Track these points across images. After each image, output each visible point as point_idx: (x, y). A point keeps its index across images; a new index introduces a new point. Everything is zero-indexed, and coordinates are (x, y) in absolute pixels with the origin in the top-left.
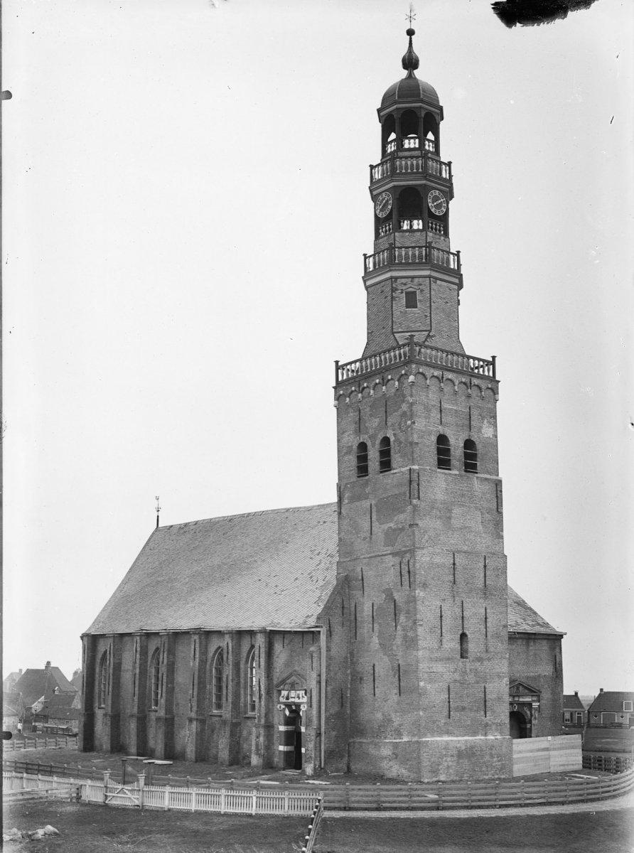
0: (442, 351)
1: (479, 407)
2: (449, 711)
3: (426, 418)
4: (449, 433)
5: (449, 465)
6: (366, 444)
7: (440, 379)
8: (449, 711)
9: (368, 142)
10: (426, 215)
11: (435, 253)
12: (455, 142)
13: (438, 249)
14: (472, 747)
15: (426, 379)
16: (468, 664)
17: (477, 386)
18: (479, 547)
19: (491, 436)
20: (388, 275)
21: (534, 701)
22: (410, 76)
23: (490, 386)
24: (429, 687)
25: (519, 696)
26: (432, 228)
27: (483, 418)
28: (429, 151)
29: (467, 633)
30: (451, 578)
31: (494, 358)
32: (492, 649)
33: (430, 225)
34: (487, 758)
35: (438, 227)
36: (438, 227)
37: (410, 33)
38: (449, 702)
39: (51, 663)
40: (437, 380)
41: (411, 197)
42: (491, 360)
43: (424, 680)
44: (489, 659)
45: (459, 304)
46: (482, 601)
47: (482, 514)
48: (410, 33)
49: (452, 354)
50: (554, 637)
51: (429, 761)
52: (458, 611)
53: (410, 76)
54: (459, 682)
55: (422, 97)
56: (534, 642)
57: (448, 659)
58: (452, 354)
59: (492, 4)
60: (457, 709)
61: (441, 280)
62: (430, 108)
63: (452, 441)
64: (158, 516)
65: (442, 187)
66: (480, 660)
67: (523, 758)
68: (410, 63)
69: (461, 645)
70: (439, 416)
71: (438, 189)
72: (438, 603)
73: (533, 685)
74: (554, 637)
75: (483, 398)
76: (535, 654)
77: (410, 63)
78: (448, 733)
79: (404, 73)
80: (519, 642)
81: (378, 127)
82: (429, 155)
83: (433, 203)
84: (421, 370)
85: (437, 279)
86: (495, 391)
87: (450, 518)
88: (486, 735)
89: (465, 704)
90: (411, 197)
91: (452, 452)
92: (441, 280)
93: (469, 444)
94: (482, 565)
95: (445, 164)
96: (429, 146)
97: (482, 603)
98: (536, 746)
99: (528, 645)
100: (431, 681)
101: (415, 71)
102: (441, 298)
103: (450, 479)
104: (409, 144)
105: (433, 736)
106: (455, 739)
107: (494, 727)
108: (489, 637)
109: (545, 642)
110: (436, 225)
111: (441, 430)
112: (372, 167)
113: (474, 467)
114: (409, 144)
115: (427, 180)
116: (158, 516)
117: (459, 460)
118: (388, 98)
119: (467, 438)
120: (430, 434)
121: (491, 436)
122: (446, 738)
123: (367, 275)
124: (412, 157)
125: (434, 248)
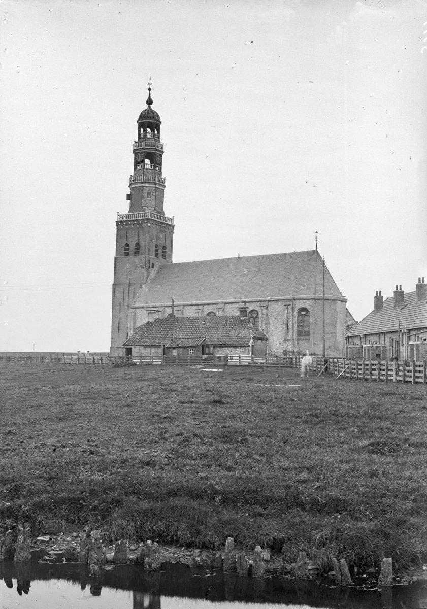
6: (92, 592)
9: (132, 133)
10: (155, 162)
22: (149, 107)
37: (150, 90)
41: (148, 155)
45: (115, 258)
48: (150, 90)
53: (149, 107)
59: (21, 594)
68: (150, 102)
77: (150, 102)
79: (147, 106)
81: (137, 125)
86: (173, 230)
90: (148, 155)
93: (137, 244)
112: (135, 142)
113: (308, 334)
118: (141, 117)
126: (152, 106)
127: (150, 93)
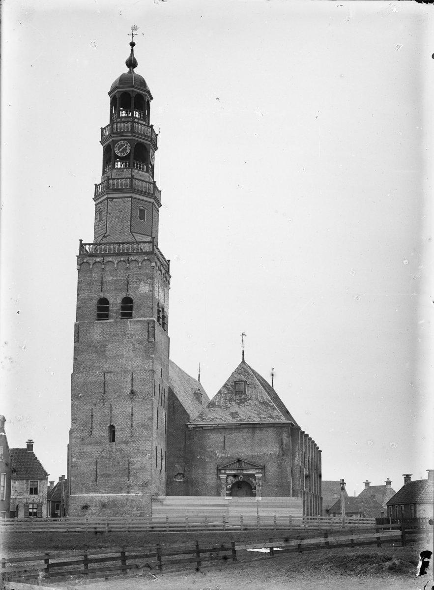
1: (137, 274)
2: (97, 477)
3: (88, 290)
4: (109, 296)
7: (102, 263)
8: (97, 477)
9: (100, 113)
11: (136, 182)
13: (138, 180)
14: (113, 501)
15: (90, 265)
16: (114, 447)
17: (135, 260)
18: (129, 367)
19: (147, 292)
21: (257, 473)
23: (146, 258)
24: (79, 462)
25: (243, 470)
26: (137, 167)
27: (140, 281)
28: (136, 118)
29: (115, 425)
30: (102, 390)
32: (137, 435)
33: (135, 165)
34: (128, 508)
35: (138, 166)
36: (138, 166)
37: (133, 44)
38: (96, 471)
40: (100, 264)
43: (76, 457)
44: (134, 442)
46: (129, 403)
47: (134, 345)
48: (133, 44)
49: (123, 243)
50: (280, 425)
51: (76, 509)
52: (107, 411)
53: (130, 72)
54: (106, 458)
55: (133, 84)
56: (260, 430)
57: (97, 443)
58: (123, 243)
60: (103, 475)
61: (116, 198)
63: (111, 301)
64: (199, 375)
65: (125, 138)
66: (126, 442)
67: (164, 509)
68: (132, 63)
70: (100, 287)
71: (122, 140)
72: (90, 407)
73: (258, 461)
74: (280, 425)
75: (140, 268)
76: (260, 439)
77: (132, 63)
78: (95, 491)
80: (245, 431)
82: (136, 120)
84: (85, 261)
85: (113, 198)
87: (104, 351)
88: (128, 492)
89: (111, 472)
91: (110, 308)
92: (116, 198)
94: (129, 379)
96: (136, 115)
97: (129, 404)
98: (186, 502)
99: (254, 433)
100: (81, 458)
101: (135, 70)
102: (116, 210)
103: (106, 325)
105: (82, 493)
106: (101, 495)
107: (136, 487)
108: (134, 427)
109: (271, 430)
110: (140, 165)
111: (102, 295)
115: (114, 137)
116: (199, 375)
117: (116, 312)
119: (125, 296)
120: (91, 299)
121: (147, 292)
122: (93, 494)
125: (135, 179)
126: (137, 71)
127: (132, 51)
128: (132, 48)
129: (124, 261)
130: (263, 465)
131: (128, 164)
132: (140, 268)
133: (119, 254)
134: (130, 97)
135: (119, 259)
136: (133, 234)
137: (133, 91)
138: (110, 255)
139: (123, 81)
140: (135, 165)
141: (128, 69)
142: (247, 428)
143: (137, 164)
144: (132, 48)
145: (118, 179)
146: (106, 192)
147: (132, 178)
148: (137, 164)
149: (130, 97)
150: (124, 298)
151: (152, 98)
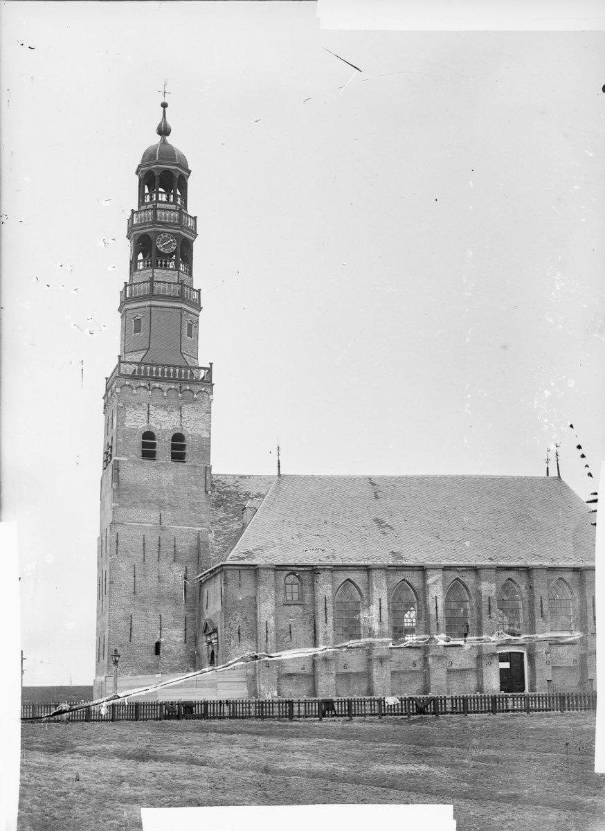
0: (163, 366)
5: (155, 456)
9: (124, 195)
12: (200, 199)
13: (159, 282)
17: (159, 388)
20: (149, 303)
22: (164, 142)
31: (211, 364)
33: (159, 263)
37: (164, 105)
39: (48, 677)
42: (209, 366)
48: (164, 105)
53: (164, 142)
62: (164, 166)
64: (548, 468)
68: (164, 131)
69: (279, 568)
77: (164, 131)
81: (136, 179)
83: (162, 244)
95: (191, 217)
104: (162, 197)
114: (162, 197)
116: (548, 468)
123: (125, 301)
124: (170, 210)
128: (164, 110)
129: (145, 387)
130: (384, 664)
131: (149, 263)
132: (164, 398)
133: (168, 380)
134: (163, 175)
135: (138, 385)
136: (145, 351)
137: (158, 168)
138: (157, 380)
139: (149, 156)
140: (159, 263)
141: (159, 137)
142: (212, 577)
143: (161, 261)
144: (164, 110)
145: (140, 283)
146: (132, 299)
147: (151, 281)
148: (161, 261)
149: (163, 175)
150: (146, 432)
151: (189, 172)
